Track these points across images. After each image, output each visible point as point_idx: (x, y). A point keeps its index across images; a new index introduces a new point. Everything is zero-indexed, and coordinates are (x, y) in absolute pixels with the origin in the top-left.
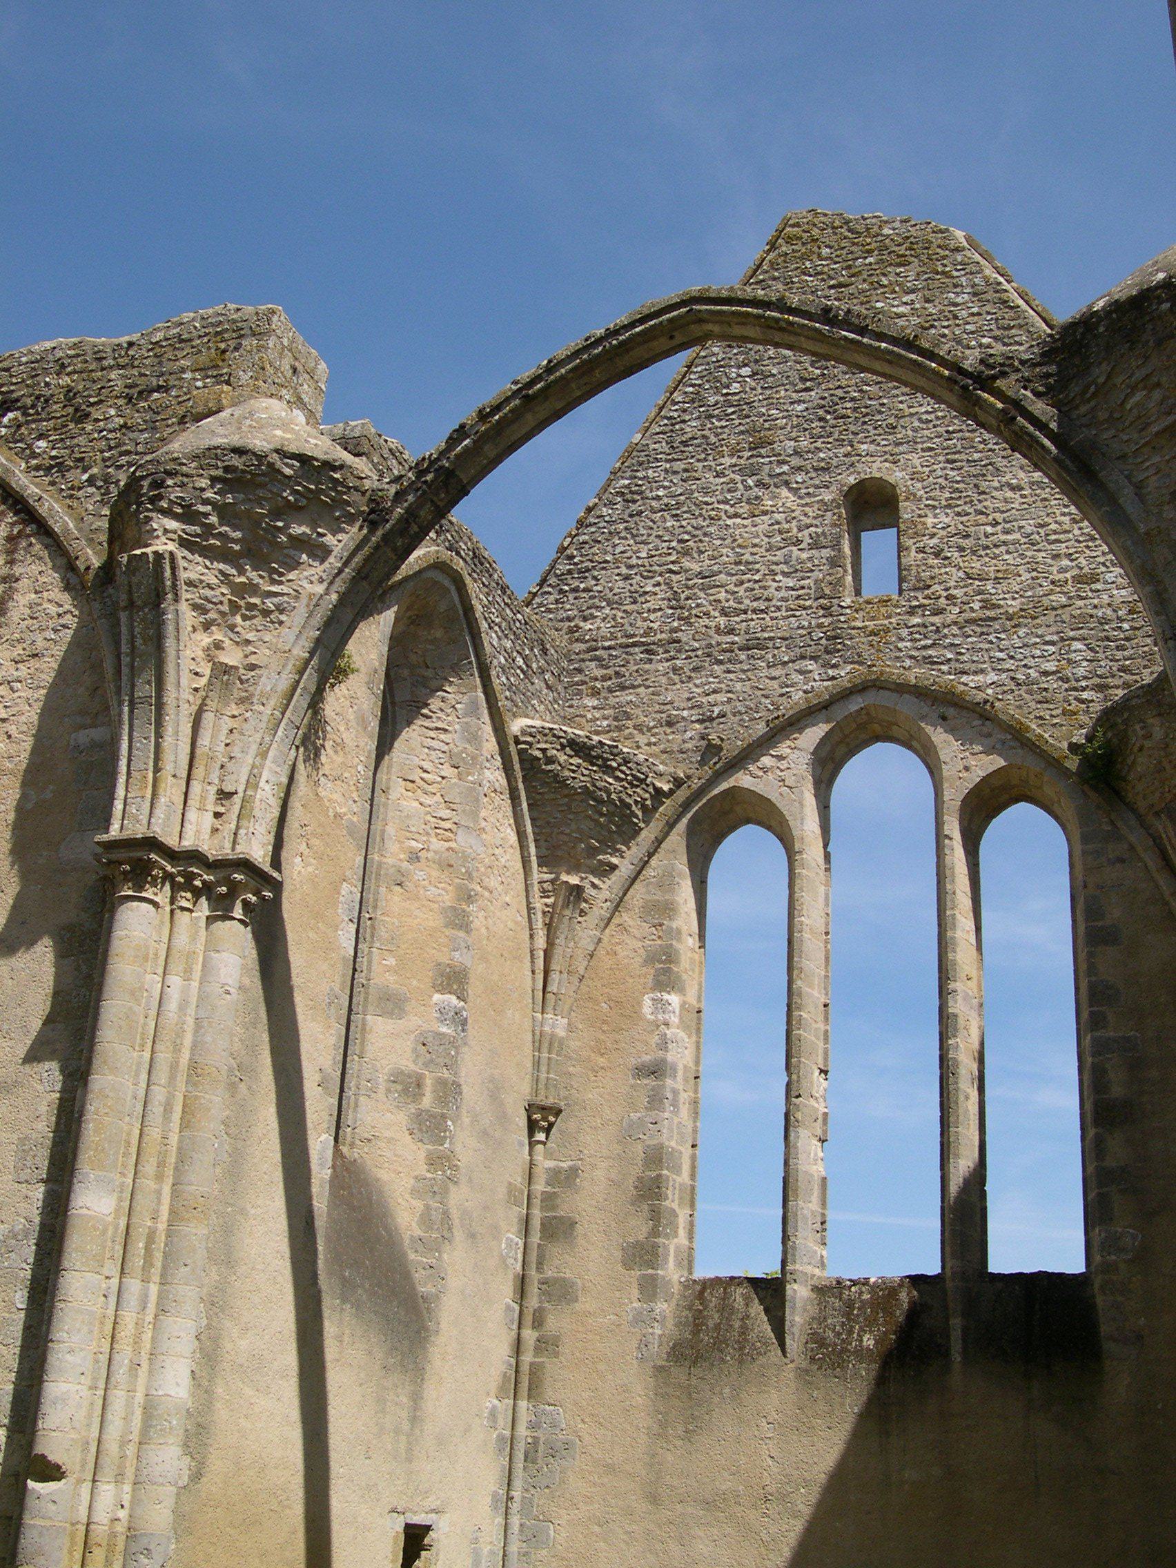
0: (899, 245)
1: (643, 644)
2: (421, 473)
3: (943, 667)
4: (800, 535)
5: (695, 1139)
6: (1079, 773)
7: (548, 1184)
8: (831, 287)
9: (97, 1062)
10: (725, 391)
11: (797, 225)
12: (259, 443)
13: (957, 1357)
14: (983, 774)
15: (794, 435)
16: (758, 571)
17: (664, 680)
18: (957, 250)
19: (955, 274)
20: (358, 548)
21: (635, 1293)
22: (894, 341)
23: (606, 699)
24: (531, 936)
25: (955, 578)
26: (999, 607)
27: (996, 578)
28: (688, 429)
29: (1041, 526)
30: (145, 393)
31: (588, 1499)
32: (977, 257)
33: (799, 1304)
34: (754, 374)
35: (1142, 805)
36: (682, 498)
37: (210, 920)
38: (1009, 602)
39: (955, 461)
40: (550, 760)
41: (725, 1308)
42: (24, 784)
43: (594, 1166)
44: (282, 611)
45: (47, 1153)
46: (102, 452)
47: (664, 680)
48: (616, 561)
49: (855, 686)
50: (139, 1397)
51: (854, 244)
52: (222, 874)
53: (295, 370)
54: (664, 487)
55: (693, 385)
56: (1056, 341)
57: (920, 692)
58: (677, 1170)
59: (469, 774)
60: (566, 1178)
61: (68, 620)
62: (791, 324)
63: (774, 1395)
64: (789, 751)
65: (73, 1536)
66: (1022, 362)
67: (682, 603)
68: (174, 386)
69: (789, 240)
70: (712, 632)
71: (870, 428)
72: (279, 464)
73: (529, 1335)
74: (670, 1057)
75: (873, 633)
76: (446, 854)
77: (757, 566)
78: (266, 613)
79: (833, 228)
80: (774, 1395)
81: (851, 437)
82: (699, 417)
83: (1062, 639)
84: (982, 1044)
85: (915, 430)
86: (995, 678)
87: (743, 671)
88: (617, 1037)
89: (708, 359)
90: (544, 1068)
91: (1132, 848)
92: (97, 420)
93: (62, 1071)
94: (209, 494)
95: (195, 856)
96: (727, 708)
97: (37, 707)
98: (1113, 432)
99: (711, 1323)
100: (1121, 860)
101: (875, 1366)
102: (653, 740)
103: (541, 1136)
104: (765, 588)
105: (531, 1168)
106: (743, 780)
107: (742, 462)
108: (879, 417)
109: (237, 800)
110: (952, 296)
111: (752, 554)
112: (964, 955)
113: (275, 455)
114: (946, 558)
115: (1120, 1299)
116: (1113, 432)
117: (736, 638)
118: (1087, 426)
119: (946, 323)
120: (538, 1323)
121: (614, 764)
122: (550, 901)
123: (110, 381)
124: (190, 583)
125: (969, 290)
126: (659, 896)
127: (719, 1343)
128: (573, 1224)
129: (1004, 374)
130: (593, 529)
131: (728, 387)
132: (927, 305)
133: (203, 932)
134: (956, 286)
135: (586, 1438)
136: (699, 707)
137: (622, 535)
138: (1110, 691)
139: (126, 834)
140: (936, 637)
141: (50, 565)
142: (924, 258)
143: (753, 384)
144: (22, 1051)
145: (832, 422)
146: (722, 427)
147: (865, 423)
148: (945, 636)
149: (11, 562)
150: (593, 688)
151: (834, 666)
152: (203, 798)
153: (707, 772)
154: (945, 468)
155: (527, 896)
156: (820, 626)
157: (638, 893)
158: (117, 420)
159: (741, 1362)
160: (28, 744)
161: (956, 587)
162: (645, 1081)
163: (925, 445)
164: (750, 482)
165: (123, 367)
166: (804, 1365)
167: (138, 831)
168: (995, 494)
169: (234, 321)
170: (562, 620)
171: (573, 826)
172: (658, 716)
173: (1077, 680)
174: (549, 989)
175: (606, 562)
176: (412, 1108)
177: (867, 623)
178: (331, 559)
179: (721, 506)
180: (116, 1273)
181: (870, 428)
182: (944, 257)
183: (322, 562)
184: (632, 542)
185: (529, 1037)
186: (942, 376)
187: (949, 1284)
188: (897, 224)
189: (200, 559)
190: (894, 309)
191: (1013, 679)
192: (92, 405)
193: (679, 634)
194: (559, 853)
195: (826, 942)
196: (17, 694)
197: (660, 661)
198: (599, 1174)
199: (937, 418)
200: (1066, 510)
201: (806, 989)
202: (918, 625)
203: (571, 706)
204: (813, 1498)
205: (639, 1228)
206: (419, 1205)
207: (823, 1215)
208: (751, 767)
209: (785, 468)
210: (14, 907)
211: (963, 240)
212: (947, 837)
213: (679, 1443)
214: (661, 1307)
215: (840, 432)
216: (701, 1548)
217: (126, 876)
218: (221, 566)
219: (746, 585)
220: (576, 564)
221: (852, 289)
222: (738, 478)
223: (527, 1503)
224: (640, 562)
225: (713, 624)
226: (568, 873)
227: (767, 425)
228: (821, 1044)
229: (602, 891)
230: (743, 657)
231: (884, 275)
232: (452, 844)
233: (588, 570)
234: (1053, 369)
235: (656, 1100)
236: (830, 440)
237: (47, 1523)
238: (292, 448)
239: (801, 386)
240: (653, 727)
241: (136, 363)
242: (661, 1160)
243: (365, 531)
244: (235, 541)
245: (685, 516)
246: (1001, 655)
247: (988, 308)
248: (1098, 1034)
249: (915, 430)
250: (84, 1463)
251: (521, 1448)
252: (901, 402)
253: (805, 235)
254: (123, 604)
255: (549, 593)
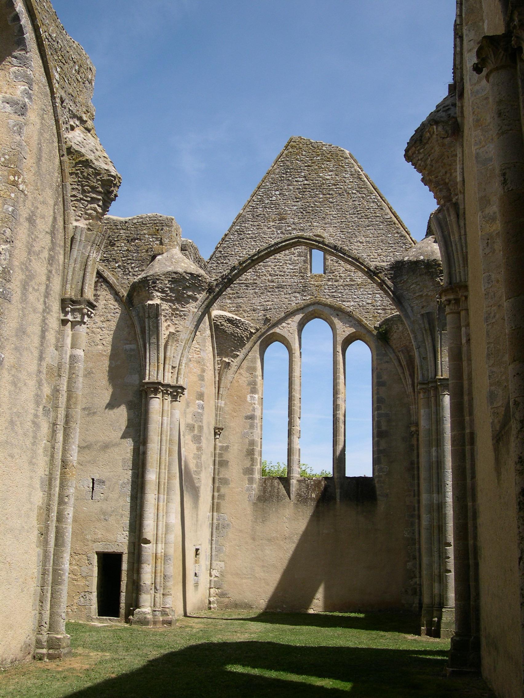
0: (328, 154)
1: (245, 283)
2: (223, 279)
3: (338, 299)
4: (294, 251)
5: (261, 437)
6: (377, 336)
7: (220, 450)
8: (306, 166)
9: (149, 441)
10: (271, 199)
11: (295, 142)
12: (180, 270)
13: (338, 500)
14: (349, 333)
15: (293, 217)
16: (281, 262)
17: (252, 296)
18: (346, 158)
19: (346, 167)
20: (206, 299)
21: (247, 482)
22: (353, 258)
23: (234, 301)
24: (215, 377)
25: (342, 270)
26: (355, 281)
27: (354, 272)
28: (259, 211)
29: (369, 256)
30: (134, 240)
31: (235, 539)
32: (353, 162)
33: (294, 485)
34: (280, 194)
35: (394, 347)
36: (257, 235)
37: (172, 401)
38: (358, 280)
39: (343, 232)
40: (222, 325)
41: (272, 486)
42: (110, 360)
43: (234, 445)
44: (185, 316)
45: (131, 462)
46: (122, 258)
47: (252, 296)
48: (236, 254)
49: (312, 303)
50: (164, 524)
51: (313, 151)
52: (175, 389)
53: (177, 235)
54: (251, 231)
55: (260, 196)
56: (394, 265)
57: (331, 307)
58: (257, 446)
59: (203, 334)
60: (225, 449)
61: (117, 310)
62: (326, 249)
63: (287, 510)
64: (291, 322)
65: (153, 556)
66: (385, 269)
67: (257, 271)
68: (143, 239)
69: (292, 147)
70: (267, 281)
71: (317, 217)
72: (185, 276)
73: (216, 494)
74: (256, 414)
75: (317, 286)
76: (198, 359)
77: (281, 261)
78: (181, 316)
79: (307, 145)
80: (287, 510)
81: (311, 220)
82: (262, 207)
83: (373, 293)
84: (345, 412)
85: (331, 220)
86: (353, 304)
87: (277, 295)
88: (240, 407)
89: (265, 187)
90: (218, 416)
91: (390, 358)
92: (118, 247)
93: (133, 441)
94: (168, 285)
95: (169, 386)
96: (272, 307)
97: (111, 337)
98: (406, 293)
99: (268, 490)
100: (388, 362)
101: (315, 502)
102: (249, 315)
103: (218, 436)
104: (283, 268)
105: (215, 446)
106: (277, 330)
107: (276, 224)
108: (320, 214)
109: (177, 369)
110: (344, 174)
111: (279, 256)
112: (341, 387)
113: (184, 273)
114: (340, 264)
115: (383, 485)
116: (406, 293)
117: (275, 284)
118: (401, 290)
119: (342, 184)
120: (218, 491)
121: (240, 325)
122: (220, 366)
123: (120, 234)
124: (163, 310)
125: (349, 173)
126: (251, 365)
127: (271, 496)
128: (228, 462)
129: (381, 272)
130: (228, 243)
131: (271, 198)
132: (336, 177)
133: (170, 405)
134: (345, 171)
135: (234, 523)
136: (263, 306)
137: (237, 245)
138: (387, 311)
139: (151, 381)
140: (336, 289)
141: (109, 292)
142: (336, 159)
143: (280, 198)
144: (120, 435)
145: (305, 214)
146: (270, 212)
147: (315, 215)
148: (339, 289)
149: (96, 290)
150: (229, 297)
151: (305, 296)
152: (169, 369)
153: (266, 327)
154: (340, 234)
155: (214, 366)
156: (301, 282)
157: (245, 363)
158: (125, 247)
159: (278, 501)
160: (110, 348)
161: (342, 273)
162: (249, 421)
163: (334, 225)
164: (279, 232)
165: (124, 230)
166: (296, 502)
167: (153, 379)
168: (355, 244)
169: (160, 220)
170: (218, 273)
171: (227, 344)
172: (250, 307)
173: (377, 306)
174: (220, 393)
175: (232, 254)
176: (192, 434)
177: (315, 283)
178: (198, 302)
179: (269, 239)
180: (157, 494)
181: (317, 217)
182: (342, 160)
183: (196, 302)
184: (240, 248)
185: (214, 408)
186: (365, 271)
187: (336, 480)
188: (327, 146)
189: (165, 303)
190: (326, 177)
191: (358, 304)
192: (116, 241)
193: (257, 281)
194: (223, 352)
195: (300, 379)
196: (104, 332)
197: (251, 289)
198: (235, 447)
199: (338, 216)
200: (376, 251)
201: (296, 395)
202: (331, 285)
203: (222, 302)
204: (299, 538)
205: (248, 464)
206: (195, 461)
207: (299, 459)
208: (279, 326)
209: (290, 228)
210: (112, 395)
211: (348, 155)
212: (338, 352)
213: (261, 524)
214: (255, 486)
215: (308, 218)
216: (268, 552)
217: (152, 392)
218: (170, 304)
219: (277, 267)
220: (222, 254)
221: (312, 168)
222: (275, 230)
223: (217, 541)
224: (243, 255)
225: (267, 279)
226: (225, 358)
227: (284, 213)
228: (299, 410)
229: (235, 363)
230: (277, 291)
231: (323, 164)
232: (200, 356)
233: (226, 257)
234: (393, 272)
235: (252, 426)
236: (304, 220)
237: (148, 554)
238: (188, 271)
239: (295, 200)
240: (249, 311)
241: (129, 229)
242: (254, 444)
243: (208, 295)
244: (173, 297)
245: (258, 241)
246: (355, 297)
247: (355, 180)
248: (379, 412)
249: (331, 220)
250: (154, 539)
251: (215, 526)
252: (327, 210)
253: (298, 146)
254: (146, 317)
255: (214, 263)
